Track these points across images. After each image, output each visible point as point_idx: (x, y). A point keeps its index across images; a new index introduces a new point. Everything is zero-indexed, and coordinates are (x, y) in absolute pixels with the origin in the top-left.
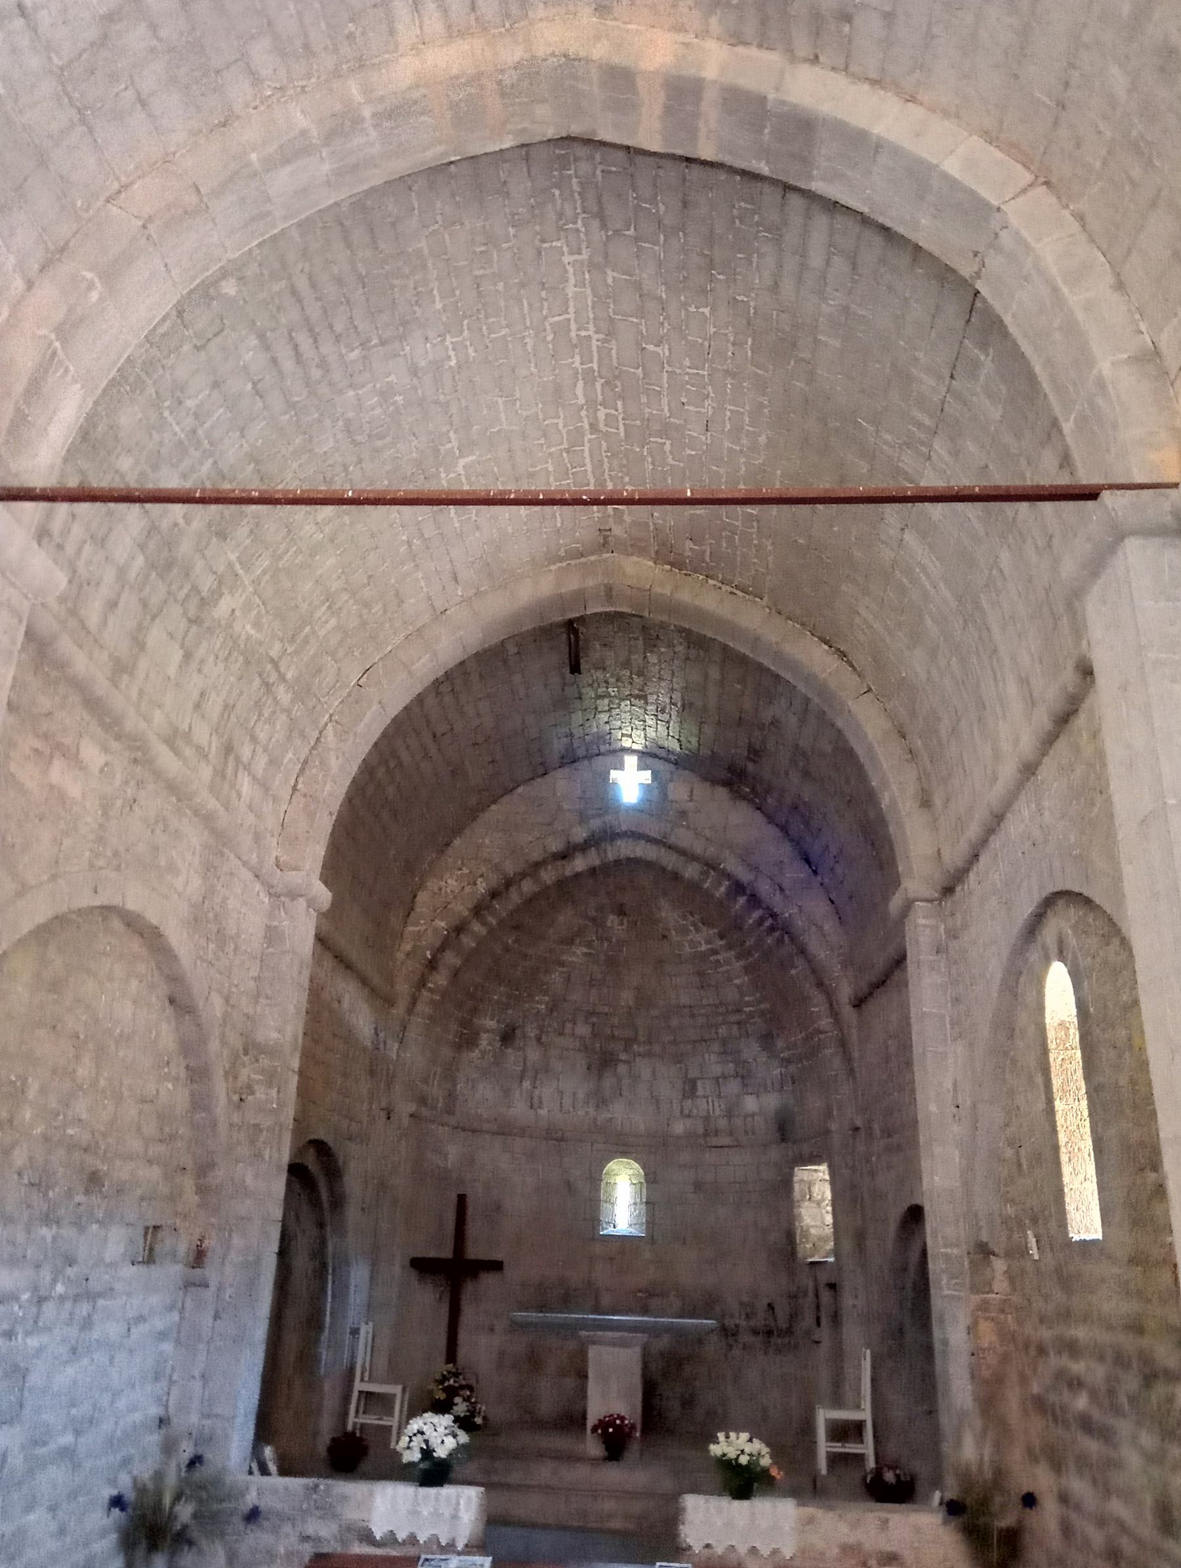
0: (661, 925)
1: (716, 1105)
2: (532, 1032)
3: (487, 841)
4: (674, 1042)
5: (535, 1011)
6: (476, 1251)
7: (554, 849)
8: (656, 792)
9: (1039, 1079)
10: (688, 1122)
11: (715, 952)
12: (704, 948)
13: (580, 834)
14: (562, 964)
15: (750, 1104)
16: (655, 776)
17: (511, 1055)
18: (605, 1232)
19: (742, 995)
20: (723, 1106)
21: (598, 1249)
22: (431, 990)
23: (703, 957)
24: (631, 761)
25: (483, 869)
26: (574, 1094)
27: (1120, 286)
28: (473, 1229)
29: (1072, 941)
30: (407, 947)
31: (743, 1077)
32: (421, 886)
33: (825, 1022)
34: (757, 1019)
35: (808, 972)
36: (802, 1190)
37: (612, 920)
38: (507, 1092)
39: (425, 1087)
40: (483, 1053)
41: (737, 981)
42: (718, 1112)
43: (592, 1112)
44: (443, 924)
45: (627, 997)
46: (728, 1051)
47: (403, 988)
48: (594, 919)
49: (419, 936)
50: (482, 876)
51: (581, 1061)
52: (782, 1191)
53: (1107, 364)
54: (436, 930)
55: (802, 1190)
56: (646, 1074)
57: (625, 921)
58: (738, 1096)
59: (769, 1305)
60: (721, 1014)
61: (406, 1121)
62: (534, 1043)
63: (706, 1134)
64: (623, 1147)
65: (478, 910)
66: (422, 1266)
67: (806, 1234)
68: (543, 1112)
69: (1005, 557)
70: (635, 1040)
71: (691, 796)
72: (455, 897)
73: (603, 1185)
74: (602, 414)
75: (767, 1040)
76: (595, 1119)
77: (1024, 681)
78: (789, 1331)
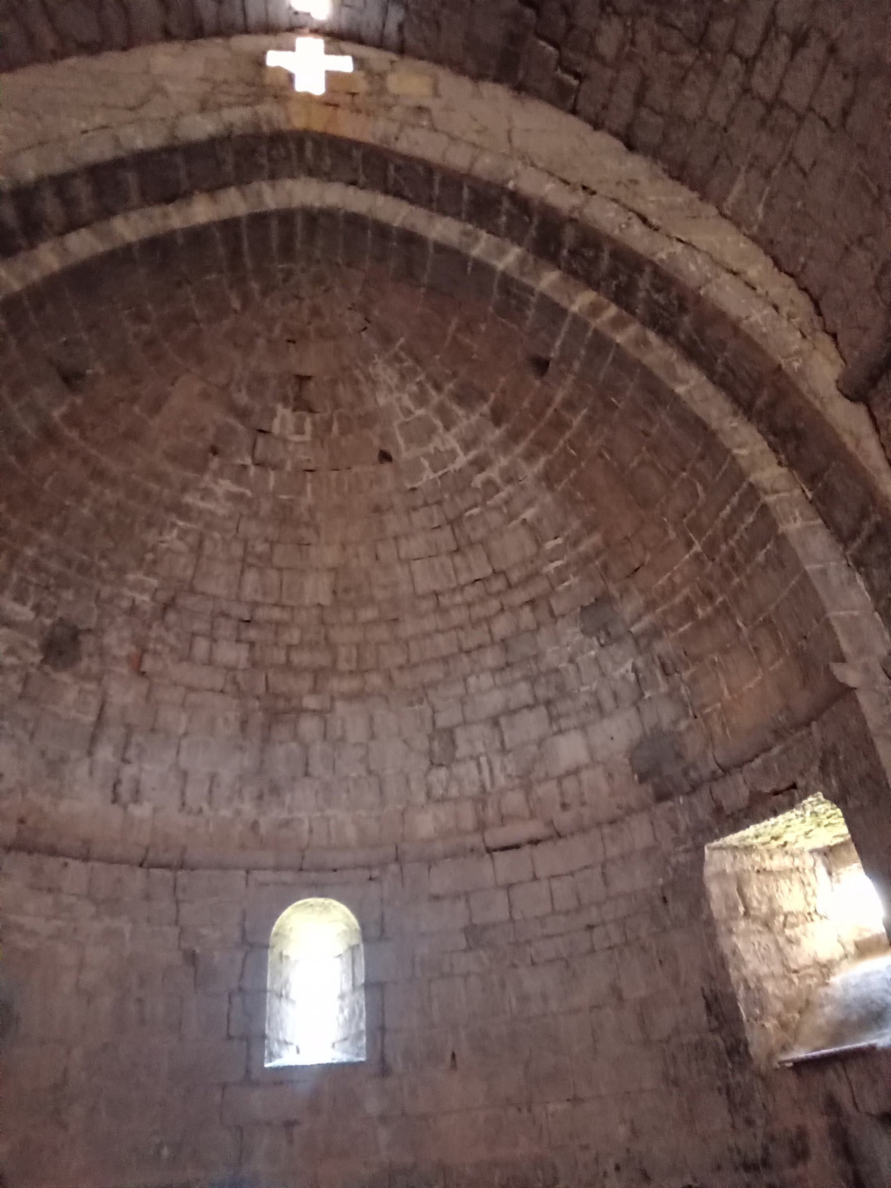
0: (378, 428)
2: (118, 640)
4: (408, 666)
5: (125, 604)
10: (444, 813)
11: (480, 464)
14: (184, 512)
15: (570, 749)
17: (71, 694)
18: (277, 1063)
19: (539, 543)
20: (510, 768)
21: (256, 1102)
23: (460, 484)
26: (213, 778)
31: (548, 703)
34: (573, 580)
35: (710, 389)
36: (727, 896)
37: (284, 418)
38: (55, 766)
41: (529, 514)
42: (501, 781)
43: (248, 808)
45: (316, 589)
46: (511, 658)
48: (243, 414)
51: (228, 711)
55: (727, 896)
56: (357, 732)
57: (308, 427)
60: (499, 593)
62: (124, 670)
63: (482, 826)
64: (315, 876)
67: (758, 997)
68: (141, 811)
70: (333, 669)
73: (272, 957)
75: (597, 616)
76: (255, 826)
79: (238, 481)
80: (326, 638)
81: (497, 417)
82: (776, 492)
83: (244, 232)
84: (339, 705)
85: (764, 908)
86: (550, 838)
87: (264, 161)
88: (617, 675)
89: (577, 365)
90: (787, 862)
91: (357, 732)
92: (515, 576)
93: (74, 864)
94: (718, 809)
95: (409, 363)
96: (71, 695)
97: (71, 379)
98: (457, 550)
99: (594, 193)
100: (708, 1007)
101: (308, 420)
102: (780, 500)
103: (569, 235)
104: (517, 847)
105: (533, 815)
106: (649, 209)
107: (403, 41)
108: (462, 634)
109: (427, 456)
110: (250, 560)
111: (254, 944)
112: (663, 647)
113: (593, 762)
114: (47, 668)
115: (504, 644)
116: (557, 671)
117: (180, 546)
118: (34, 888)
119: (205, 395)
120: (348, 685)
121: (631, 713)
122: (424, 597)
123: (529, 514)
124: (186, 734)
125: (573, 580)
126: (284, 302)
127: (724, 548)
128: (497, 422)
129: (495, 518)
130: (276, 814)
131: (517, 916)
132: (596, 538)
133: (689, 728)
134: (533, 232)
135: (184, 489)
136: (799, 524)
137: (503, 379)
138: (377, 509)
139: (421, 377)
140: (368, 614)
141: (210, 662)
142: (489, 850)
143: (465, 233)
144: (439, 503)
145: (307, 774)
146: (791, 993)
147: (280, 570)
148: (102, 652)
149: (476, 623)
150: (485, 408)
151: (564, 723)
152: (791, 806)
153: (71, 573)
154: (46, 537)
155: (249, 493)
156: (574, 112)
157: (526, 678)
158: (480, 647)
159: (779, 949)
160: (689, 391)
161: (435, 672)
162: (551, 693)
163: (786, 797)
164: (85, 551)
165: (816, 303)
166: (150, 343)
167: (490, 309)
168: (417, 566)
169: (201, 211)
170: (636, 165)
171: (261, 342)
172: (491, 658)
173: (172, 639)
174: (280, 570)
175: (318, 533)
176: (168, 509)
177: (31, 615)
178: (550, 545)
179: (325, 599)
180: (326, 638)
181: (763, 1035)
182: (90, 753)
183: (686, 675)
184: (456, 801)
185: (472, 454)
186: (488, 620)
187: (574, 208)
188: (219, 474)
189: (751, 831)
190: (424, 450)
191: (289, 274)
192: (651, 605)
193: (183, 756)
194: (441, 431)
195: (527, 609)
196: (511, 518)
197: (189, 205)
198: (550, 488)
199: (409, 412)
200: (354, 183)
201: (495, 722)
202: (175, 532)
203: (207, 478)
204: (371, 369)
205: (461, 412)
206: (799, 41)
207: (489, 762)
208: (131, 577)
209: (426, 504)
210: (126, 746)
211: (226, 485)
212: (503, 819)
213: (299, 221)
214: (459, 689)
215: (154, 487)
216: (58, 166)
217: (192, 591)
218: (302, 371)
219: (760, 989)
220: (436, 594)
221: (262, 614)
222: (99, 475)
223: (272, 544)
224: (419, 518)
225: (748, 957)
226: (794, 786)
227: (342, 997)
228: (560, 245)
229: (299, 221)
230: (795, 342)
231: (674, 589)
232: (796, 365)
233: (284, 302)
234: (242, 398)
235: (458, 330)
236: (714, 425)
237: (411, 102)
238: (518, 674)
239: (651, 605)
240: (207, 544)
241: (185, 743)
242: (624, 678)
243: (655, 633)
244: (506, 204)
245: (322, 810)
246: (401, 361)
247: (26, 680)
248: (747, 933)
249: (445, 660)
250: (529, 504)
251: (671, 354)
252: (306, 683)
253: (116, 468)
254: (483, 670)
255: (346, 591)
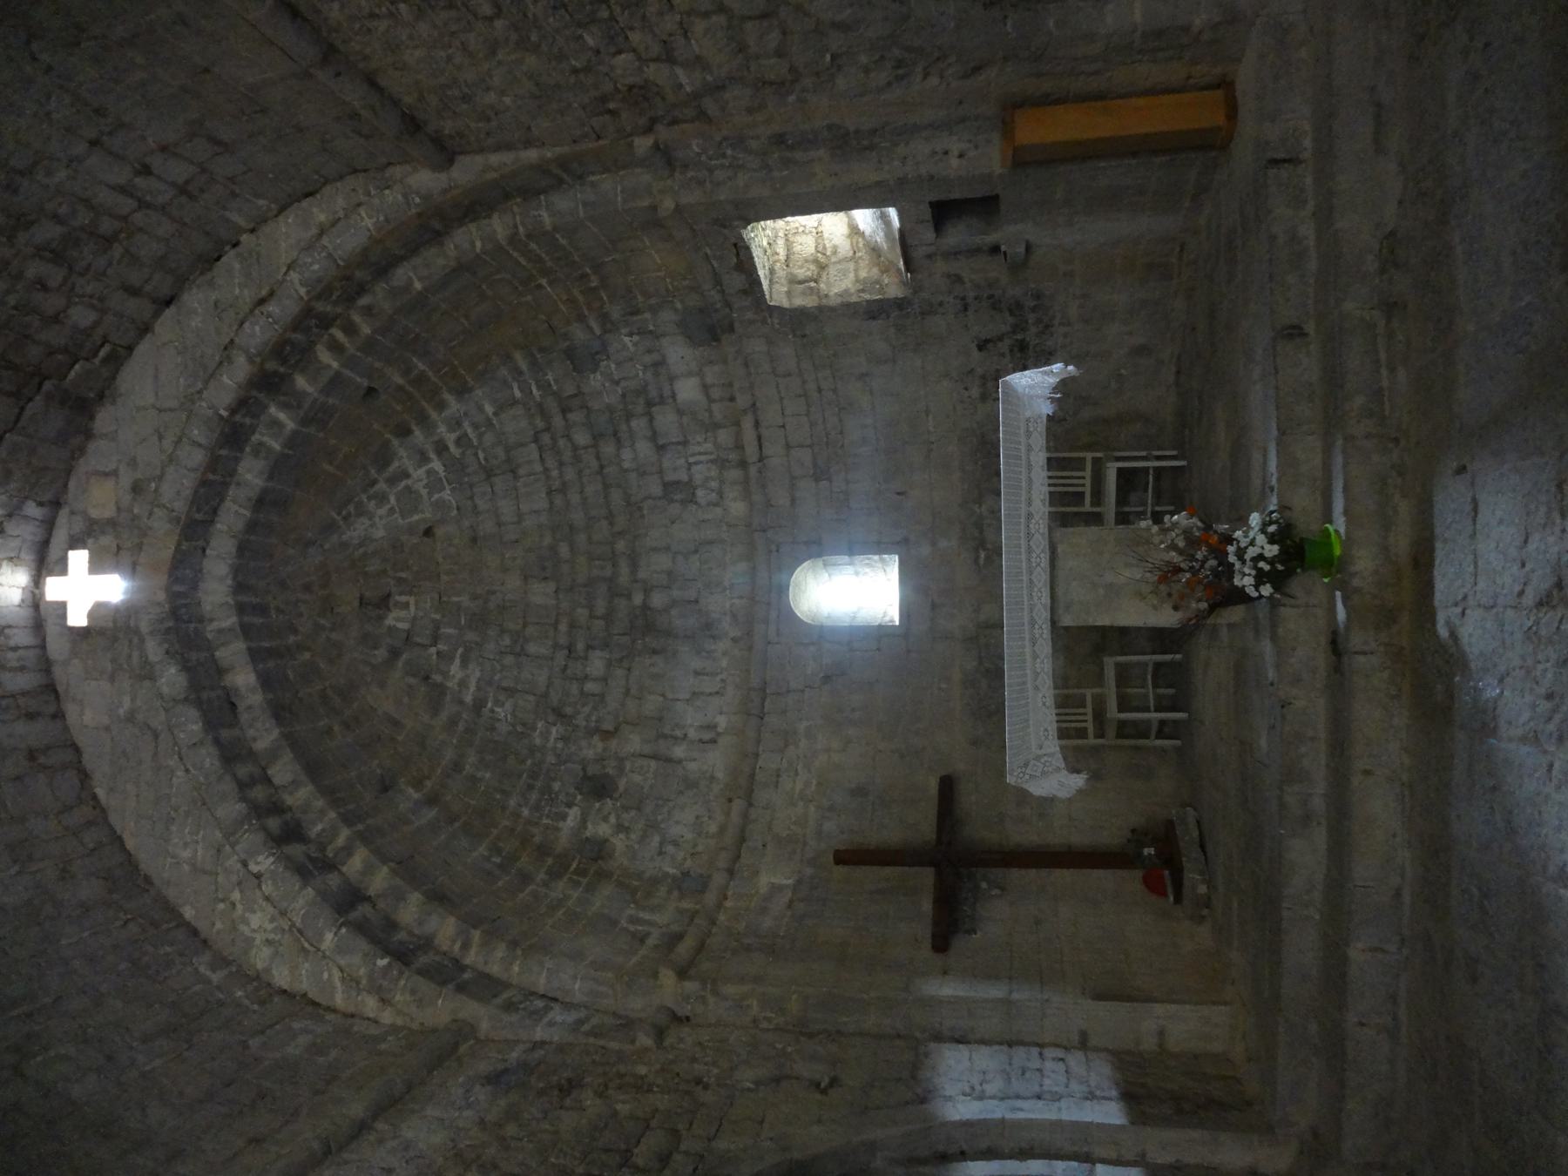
1: (698, 449)
2: (591, 749)
3: (186, 854)
4: (610, 517)
5: (560, 745)
6: (922, 825)
7: (196, 727)
8: (107, 540)
11: (441, 448)
13: (172, 678)
14: (479, 705)
15: (688, 390)
16: (75, 543)
20: (699, 438)
22: (466, 946)
24: (54, 588)
25: (233, 862)
26: (697, 673)
28: (888, 833)
30: (370, 1005)
32: (260, 984)
33: (498, 226)
35: (416, 261)
36: (803, 293)
37: (396, 619)
38: (690, 784)
39: (651, 942)
40: (621, 828)
41: (489, 409)
42: (709, 446)
43: (722, 645)
44: (329, 936)
45: (541, 594)
47: (443, 1009)
48: (395, 654)
49: (351, 981)
50: (245, 864)
52: (810, 324)
54: (340, 949)
55: (803, 293)
56: (662, 562)
57: (403, 599)
58: (680, 412)
59: (980, 348)
61: (691, 986)
62: (613, 743)
65: (314, 866)
66: (948, 926)
67: (865, 285)
68: (722, 722)
71: (106, 475)
72: (283, 913)
75: (580, 361)
76: (734, 640)
78: (1016, 308)
79: (452, 659)
80: (585, 586)
81: (404, 432)
82: (516, 226)
83: (253, 645)
84: (642, 575)
85: (812, 267)
86: (755, 412)
87: (192, 626)
88: (632, 349)
89: (377, 365)
90: (781, 242)
91: (662, 562)
92: (540, 424)
93: (760, 763)
94: (745, 292)
95: (351, 508)
96: (637, 778)
97: (386, 786)
98: (512, 471)
99: (232, 341)
100: (874, 318)
101: (398, 598)
102: (523, 224)
103: (271, 366)
104: (759, 438)
105: (737, 424)
106: (248, 296)
107: (50, 502)
108: (587, 472)
109: (430, 494)
110: (518, 649)
111: (820, 635)
112: (615, 312)
113: (700, 374)
114: (616, 795)
115: (597, 437)
116: (624, 395)
117: (508, 705)
118: (777, 785)
119: (382, 685)
120: (624, 570)
121: (665, 341)
122: (551, 503)
123: (489, 409)
124: (663, 695)
125: (550, 377)
126: (301, 615)
127: (549, 264)
128: (409, 432)
129: (489, 438)
130: (726, 624)
131: (809, 442)
132: (518, 356)
133: (682, 302)
134: (261, 396)
135: (461, 702)
136: (545, 214)
137: (375, 426)
138: (474, 540)
139: (364, 497)
140: (564, 550)
141: (605, 679)
142: (760, 460)
143: (256, 453)
144: (471, 486)
145: (697, 601)
146: (867, 257)
147: (525, 625)
148: (601, 760)
149: (577, 459)
150: (395, 442)
151: (667, 393)
152: (748, 249)
153: (539, 784)
154: (512, 803)
155: (460, 650)
156: (130, 349)
157: (628, 421)
158: (598, 458)
159: (839, 262)
160: (420, 279)
161: (616, 496)
162: (641, 401)
163: (742, 254)
164: (520, 776)
165: (355, 171)
166: (346, 726)
167: (321, 435)
168: (524, 507)
169: (243, 679)
170: (195, 299)
171: (334, 636)
172: (608, 449)
173: (587, 709)
174: (525, 625)
175: (494, 593)
176: (479, 715)
177: (575, 809)
178: (518, 394)
179: (551, 587)
180: (585, 586)
181: (894, 289)
182: (680, 762)
183: (640, 299)
184: (722, 482)
185: (433, 456)
186: (575, 448)
187: (251, 360)
188: (445, 674)
189: (761, 273)
190: (425, 497)
191: (279, 610)
192: (581, 318)
193: (681, 696)
194: (409, 482)
195: (570, 416)
196: (490, 424)
197: (237, 690)
198: (470, 390)
199: (392, 511)
200: (204, 550)
201: (661, 449)
202: (498, 709)
203: (450, 684)
204: (356, 542)
205: (396, 464)
206: (146, 170)
207: (693, 455)
208: (538, 741)
209: (471, 498)
210: (676, 738)
211: (455, 669)
212: (739, 447)
213: (244, 598)
214: (633, 475)
215: (461, 727)
216: (228, 786)
217: (546, 695)
218: (356, 603)
219: (865, 281)
220: (549, 493)
221: (563, 640)
222: (457, 767)
223: (503, 631)
224: (482, 504)
225: (844, 287)
226: (735, 245)
227: (857, 573)
228: (275, 373)
229: (244, 598)
230: (393, 196)
231: (572, 301)
232: (417, 200)
233: (301, 615)
234: (381, 654)
235: (331, 463)
236: (453, 263)
237: (127, 499)
238: (624, 427)
239: (581, 318)
240: (505, 684)
241: (670, 696)
242: (635, 344)
243: (604, 318)
244: (238, 418)
245: (725, 589)
246: (349, 514)
247: (626, 808)
248: (828, 284)
249: (606, 486)
250: (481, 409)
251: (381, 288)
252: (622, 603)
253: (449, 755)
254: (618, 456)
255: (544, 569)
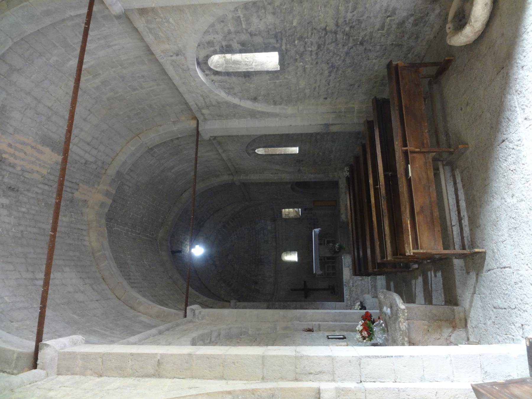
9: (273, 157)
12: (236, 236)
27: (160, 126)
29: (253, 148)
52: (288, 220)
53: (175, 128)
67: (295, 216)
69: (185, 152)
74: (137, 232)
77: (207, 151)
